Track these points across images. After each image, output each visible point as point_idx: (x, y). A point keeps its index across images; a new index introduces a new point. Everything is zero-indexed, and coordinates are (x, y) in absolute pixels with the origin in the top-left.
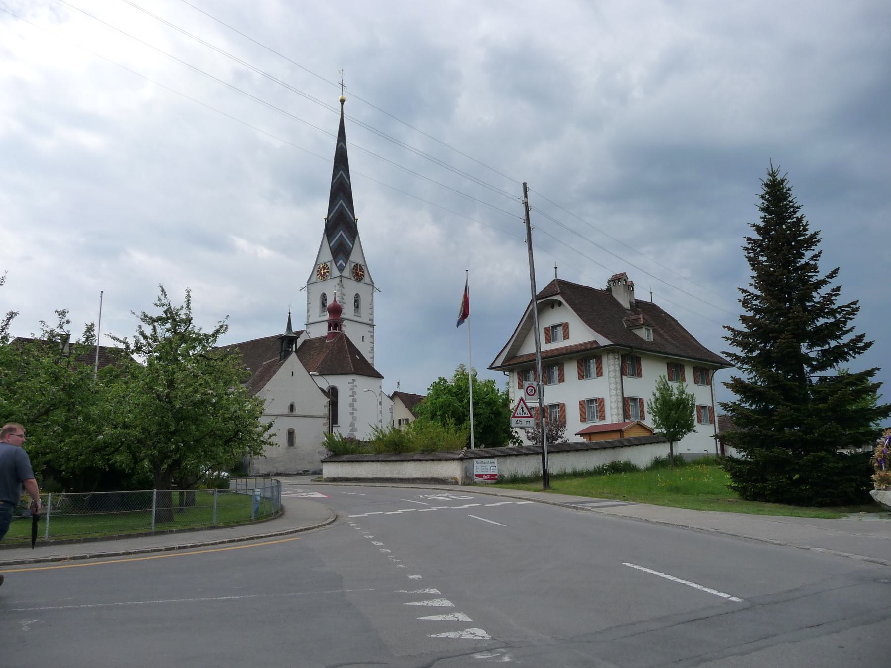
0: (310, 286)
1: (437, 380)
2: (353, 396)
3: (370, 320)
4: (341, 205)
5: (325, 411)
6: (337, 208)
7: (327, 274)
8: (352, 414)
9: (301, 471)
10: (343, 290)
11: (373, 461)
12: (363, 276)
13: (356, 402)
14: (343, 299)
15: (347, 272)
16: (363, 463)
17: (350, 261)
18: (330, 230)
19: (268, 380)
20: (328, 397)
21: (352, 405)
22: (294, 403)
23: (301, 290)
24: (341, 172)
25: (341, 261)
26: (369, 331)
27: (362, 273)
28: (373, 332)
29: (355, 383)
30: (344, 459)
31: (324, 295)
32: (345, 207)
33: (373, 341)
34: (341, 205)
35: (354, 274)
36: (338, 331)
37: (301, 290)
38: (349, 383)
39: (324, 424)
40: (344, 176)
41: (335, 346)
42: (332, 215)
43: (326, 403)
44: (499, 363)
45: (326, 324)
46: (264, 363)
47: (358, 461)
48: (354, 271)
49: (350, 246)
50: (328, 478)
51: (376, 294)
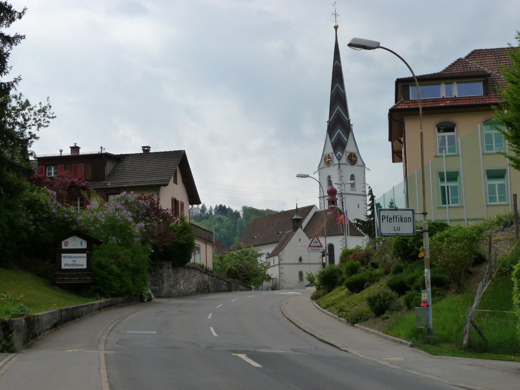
0: (320, 171)
3: (363, 192)
4: (338, 110)
7: (330, 162)
12: (357, 160)
14: (342, 180)
15: (344, 160)
17: (346, 151)
18: (331, 130)
22: (301, 256)
23: (314, 173)
24: (337, 84)
25: (339, 153)
26: (363, 200)
37: (314, 173)
38: (340, 241)
40: (339, 87)
41: (332, 217)
42: (332, 118)
43: (320, 256)
46: (286, 232)
51: (367, 172)
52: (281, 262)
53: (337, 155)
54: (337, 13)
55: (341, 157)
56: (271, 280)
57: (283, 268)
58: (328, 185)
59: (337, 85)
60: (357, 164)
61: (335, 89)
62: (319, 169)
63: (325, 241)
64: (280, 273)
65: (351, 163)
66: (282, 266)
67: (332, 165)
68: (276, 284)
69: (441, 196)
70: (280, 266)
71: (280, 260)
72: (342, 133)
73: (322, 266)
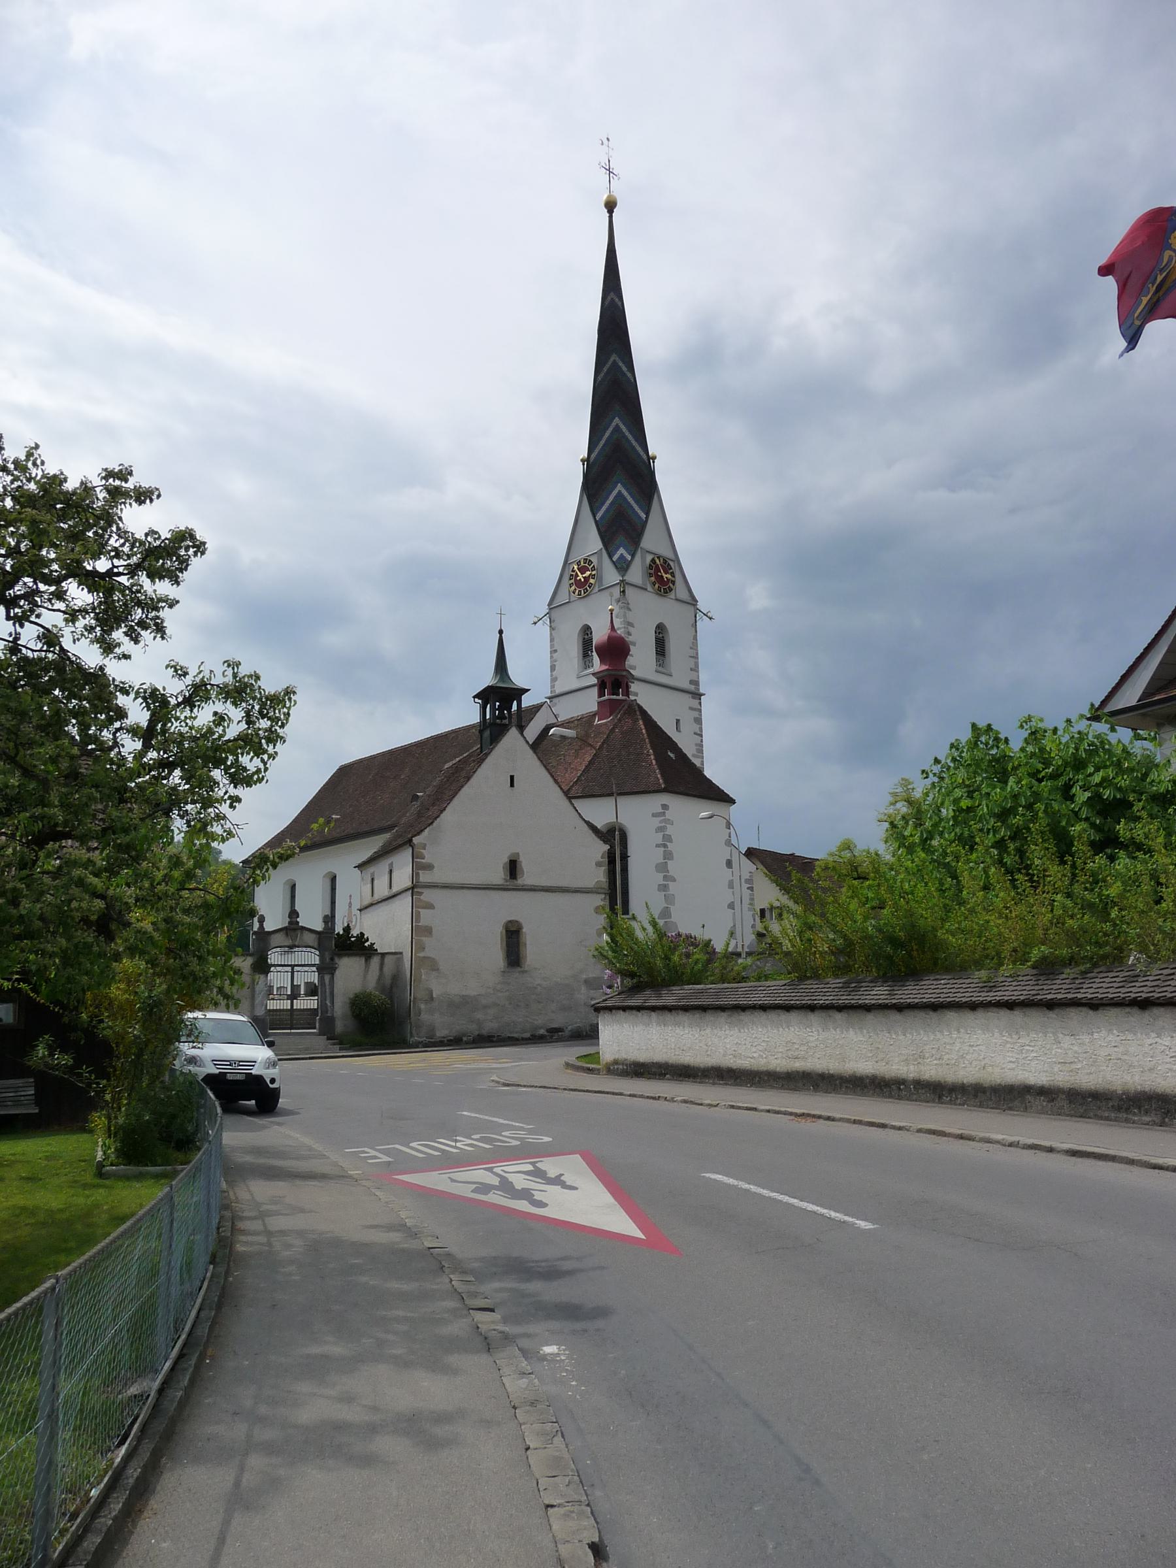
0: (555, 614)
1: (965, 736)
2: (665, 846)
3: (692, 682)
4: (617, 427)
5: (599, 876)
6: (607, 434)
7: (592, 581)
8: (663, 888)
9: (542, 1032)
10: (629, 614)
11: (788, 1008)
12: (673, 583)
13: (672, 859)
15: (636, 574)
16: (745, 1017)
19: (451, 800)
20: (605, 842)
21: (662, 868)
23: (535, 623)
24: (614, 357)
25: (622, 551)
26: (691, 709)
27: (669, 576)
28: (700, 711)
31: (586, 630)
32: (627, 434)
33: (701, 729)
35: (653, 579)
36: (620, 697)
37: (535, 623)
38: (654, 815)
39: (597, 910)
40: (621, 364)
42: (602, 375)
44: (1131, 696)
45: (595, 690)
47: (722, 1008)
48: (652, 571)
49: (640, 517)
50: (616, 1062)
52: (424, 877)
53: (615, 558)
54: (606, 173)
55: (629, 564)
56: (375, 961)
57: (430, 906)
58: (581, 657)
59: (612, 359)
60: (676, 596)
61: (605, 369)
62: (553, 611)
63: (601, 812)
64: (419, 931)
65: (657, 586)
66: (427, 895)
67: (596, 589)
68: (396, 977)
69: (231, 1062)
70: (420, 894)
71: (419, 866)
72: (630, 494)
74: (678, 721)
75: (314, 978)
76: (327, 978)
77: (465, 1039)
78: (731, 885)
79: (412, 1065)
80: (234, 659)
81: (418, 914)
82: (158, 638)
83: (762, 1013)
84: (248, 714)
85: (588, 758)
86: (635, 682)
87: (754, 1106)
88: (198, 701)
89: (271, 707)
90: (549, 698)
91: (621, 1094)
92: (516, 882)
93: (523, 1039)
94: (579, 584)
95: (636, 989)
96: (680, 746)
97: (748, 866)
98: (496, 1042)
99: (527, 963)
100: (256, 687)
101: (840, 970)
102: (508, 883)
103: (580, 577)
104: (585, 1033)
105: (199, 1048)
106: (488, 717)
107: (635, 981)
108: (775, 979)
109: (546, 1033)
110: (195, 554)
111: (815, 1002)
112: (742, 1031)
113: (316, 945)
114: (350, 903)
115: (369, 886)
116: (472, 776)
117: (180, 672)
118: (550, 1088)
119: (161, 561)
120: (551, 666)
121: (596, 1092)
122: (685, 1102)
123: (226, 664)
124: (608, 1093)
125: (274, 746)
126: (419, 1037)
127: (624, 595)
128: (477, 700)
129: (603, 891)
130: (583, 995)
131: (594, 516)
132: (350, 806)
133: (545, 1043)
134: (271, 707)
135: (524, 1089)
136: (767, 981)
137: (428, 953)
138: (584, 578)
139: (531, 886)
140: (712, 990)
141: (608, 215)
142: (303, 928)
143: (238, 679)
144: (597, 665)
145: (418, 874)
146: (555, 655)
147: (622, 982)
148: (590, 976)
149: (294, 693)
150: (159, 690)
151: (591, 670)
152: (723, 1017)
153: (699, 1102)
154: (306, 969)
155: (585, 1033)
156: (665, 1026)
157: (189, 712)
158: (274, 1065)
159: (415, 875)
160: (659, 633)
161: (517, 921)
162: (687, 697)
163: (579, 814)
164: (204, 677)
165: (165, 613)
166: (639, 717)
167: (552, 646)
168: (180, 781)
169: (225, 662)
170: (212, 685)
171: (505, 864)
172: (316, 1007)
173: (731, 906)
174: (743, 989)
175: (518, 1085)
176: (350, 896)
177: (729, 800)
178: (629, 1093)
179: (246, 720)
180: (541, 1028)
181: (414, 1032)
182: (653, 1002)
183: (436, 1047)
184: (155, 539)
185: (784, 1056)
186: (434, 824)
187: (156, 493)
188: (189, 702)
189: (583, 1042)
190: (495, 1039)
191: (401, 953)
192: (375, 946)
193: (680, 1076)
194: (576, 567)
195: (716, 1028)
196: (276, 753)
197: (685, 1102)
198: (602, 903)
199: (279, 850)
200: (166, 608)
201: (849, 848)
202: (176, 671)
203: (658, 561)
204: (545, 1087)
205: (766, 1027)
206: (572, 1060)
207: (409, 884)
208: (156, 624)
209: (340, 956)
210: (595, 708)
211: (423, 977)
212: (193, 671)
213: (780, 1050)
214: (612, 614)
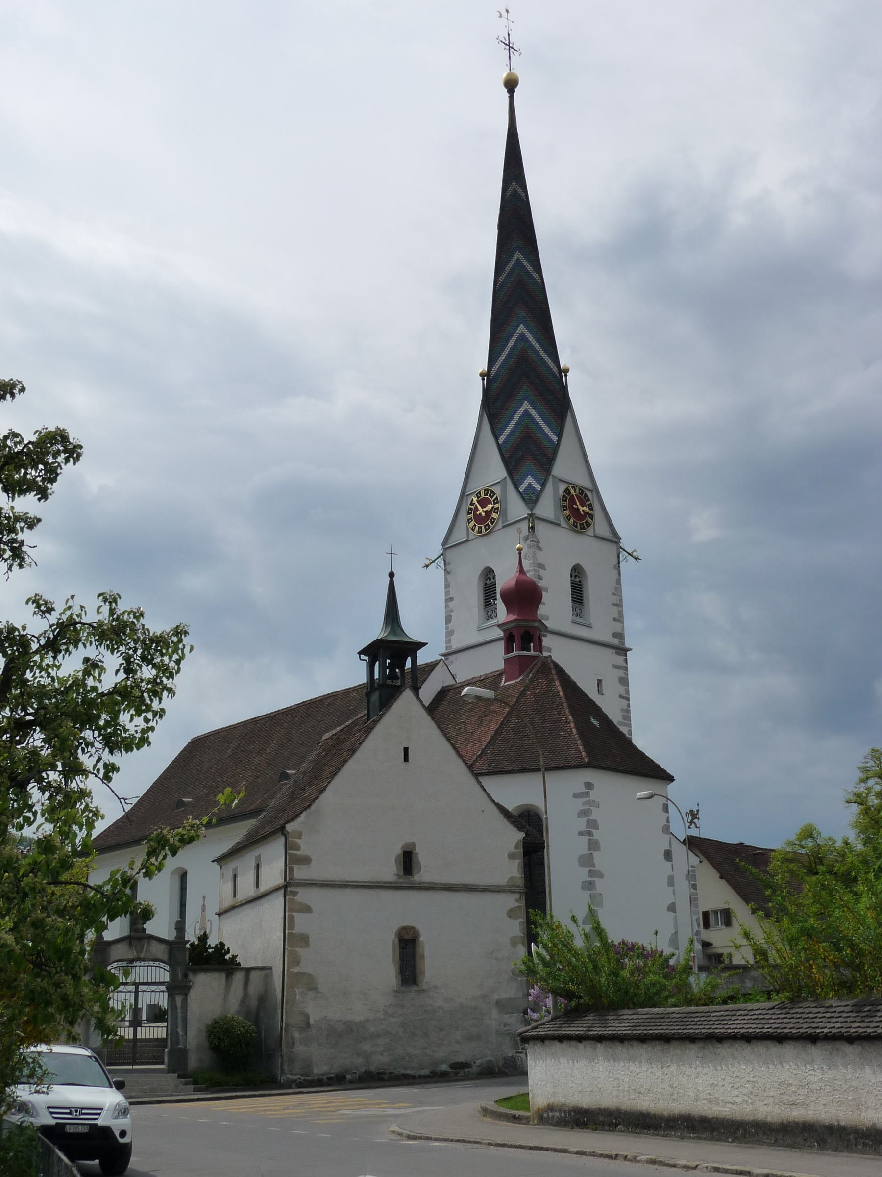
0: (449, 553)
2: (589, 833)
4: (522, 337)
7: (494, 515)
9: (444, 1067)
11: (780, 1039)
12: (592, 516)
13: (598, 850)
15: (547, 506)
16: (724, 1050)
17: (552, 476)
19: (332, 777)
20: (520, 828)
21: (587, 861)
23: (427, 566)
25: (530, 480)
26: (616, 667)
27: (586, 509)
28: (626, 669)
29: (594, 795)
30: (621, 1028)
31: (488, 574)
33: (627, 692)
34: (522, 337)
35: (567, 512)
36: (532, 653)
37: (427, 566)
38: (576, 796)
39: (511, 913)
45: (502, 644)
46: (326, 736)
47: (692, 1039)
48: (566, 504)
50: (550, 1108)
51: (627, 565)
52: (300, 873)
53: (522, 488)
56: (239, 977)
57: (307, 909)
58: (482, 607)
59: (515, 258)
65: (572, 521)
66: (304, 896)
67: (500, 525)
68: (263, 999)
69: (72, 1110)
71: (293, 860)
72: (539, 413)
73: (523, 903)
74: (600, 682)
75: (162, 1000)
76: (179, 999)
77: (349, 1077)
78: (671, 882)
79: (287, 1111)
80: (111, 591)
81: (292, 918)
82: (15, 568)
83: (745, 1045)
84: (128, 659)
85: (494, 727)
86: (548, 635)
87: (747, 1169)
88: (64, 644)
89: (156, 650)
90: (444, 655)
91: (565, 1151)
92: (411, 879)
93: (420, 1077)
94: (479, 519)
95: (573, 1014)
96: (605, 712)
97: (684, 858)
98: (388, 1080)
99: (426, 980)
100: (138, 626)
101: (845, 987)
102: (402, 880)
103: (481, 511)
104: (497, 1070)
105: (43, 1092)
106: (376, 676)
107: (573, 1003)
108: (758, 1001)
109: (449, 1069)
110: (67, 460)
111: (818, 1031)
112: (719, 1068)
113: (166, 958)
114: (204, 905)
115: (230, 885)
116: (358, 748)
117: (42, 607)
118: (470, 1142)
119: (23, 471)
120: (446, 617)
121: (531, 1148)
122: (653, 1162)
123: (101, 598)
124: (547, 1149)
125: (160, 700)
126: (291, 1074)
127: (534, 531)
128: (363, 657)
129: (518, 889)
130: (494, 1019)
131: (496, 438)
132: (204, 787)
133: (449, 1081)
134: (156, 650)
135: (436, 1144)
136: (746, 1002)
137: (305, 967)
138: (485, 512)
139: (430, 883)
140: (675, 1015)
141: (508, 95)
142: (151, 937)
143: (115, 616)
144: (502, 613)
145: (292, 870)
146: (451, 604)
147: (555, 1003)
148: (504, 996)
149: (186, 633)
150: (17, 629)
151: (494, 621)
152: (692, 1050)
153: (672, 1162)
154: (153, 988)
155: (497, 1070)
156: (615, 1060)
157: (52, 659)
158: (125, 1112)
159: (288, 870)
160: (576, 576)
161: (413, 928)
162: (610, 652)
163: (488, 795)
164: (72, 614)
165: (25, 536)
166: (555, 677)
167: (447, 593)
168: (43, 744)
169: (100, 595)
170: (84, 624)
171: (398, 856)
172: (164, 1036)
173: (672, 908)
174: (717, 1014)
175: (428, 1138)
176: (204, 897)
177: (667, 778)
178: (575, 1150)
179: (124, 668)
180: (442, 1062)
181: (286, 1067)
182: (597, 1031)
183: (312, 1087)
184: (16, 444)
185: (777, 1101)
186: (313, 807)
187: (18, 387)
188: (52, 646)
189: (495, 1080)
190: (385, 1077)
191: (270, 968)
192: (238, 960)
193: (637, 1126)
194: (475, 499)
195: (684, 1065)
196: (163, 710)
197: (653, 1162)
198: (517, 904)
199: (180, 830)
200: (25, 530)
201: (811, 836)
202: (38, 606)
203: (572, 492)
204: (464, 1141)
205: (751, 1063)
206: (491, 1105)
207: (280, 881)
208: (12, 549)
209: (196, 972)
210: (501, 666)
211: (298, 998)
212: (59, 607)
213: (772, 1094)
214: (520, 554)
